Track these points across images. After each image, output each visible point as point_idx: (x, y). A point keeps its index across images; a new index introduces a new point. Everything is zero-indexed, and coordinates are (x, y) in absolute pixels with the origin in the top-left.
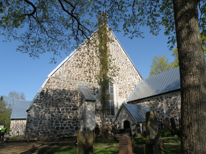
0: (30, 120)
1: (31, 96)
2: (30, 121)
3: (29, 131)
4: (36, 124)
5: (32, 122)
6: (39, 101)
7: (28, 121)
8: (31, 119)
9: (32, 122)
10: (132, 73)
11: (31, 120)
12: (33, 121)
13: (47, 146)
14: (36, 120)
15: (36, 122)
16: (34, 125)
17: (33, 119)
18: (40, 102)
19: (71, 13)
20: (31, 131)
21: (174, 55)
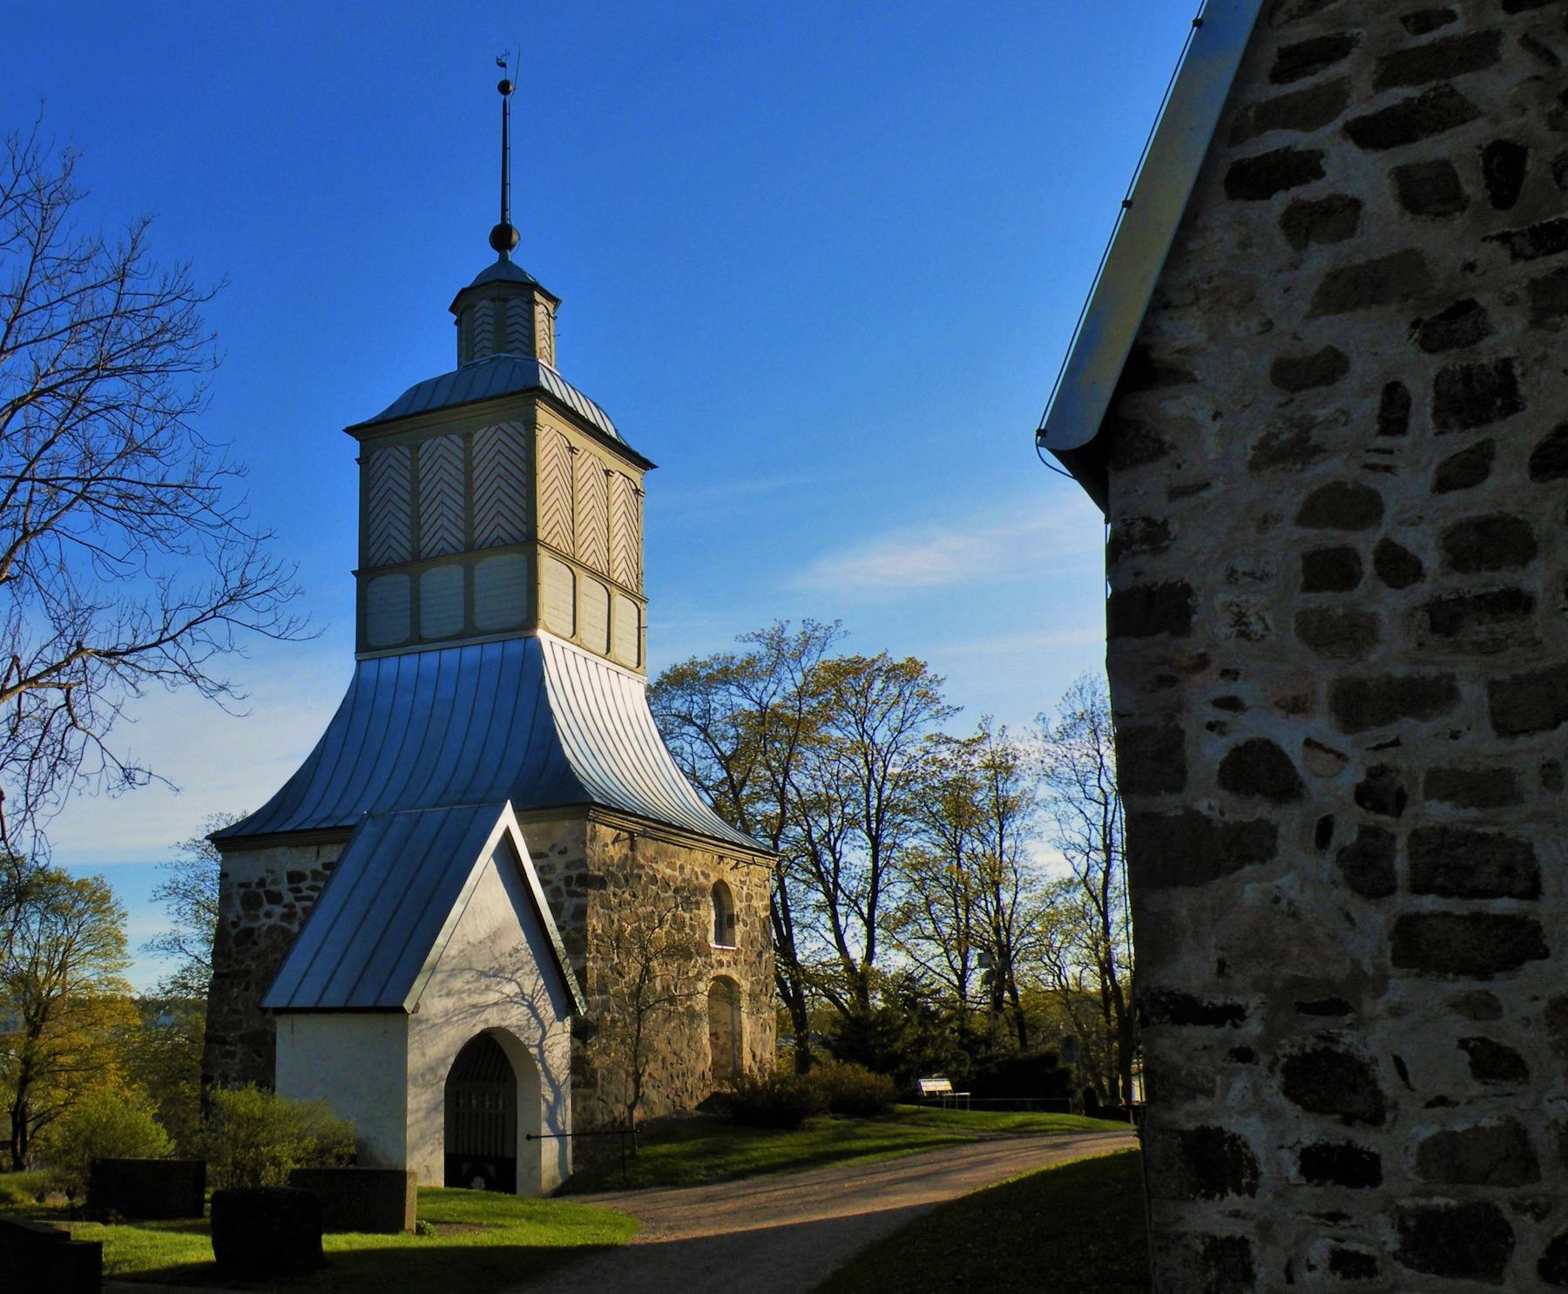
0: (1210, 753)
1: (1358, 809)
2: (1209, 801)
3: (1254, 1133)
4: (1445, 863)
5: (1290, 821)
6: (1359, 108)
7: (1168, 805)
8: (1246, 728)
9: (1290, 821)
10: (333, 1242)
11: (1259, 770)
12: (1333, 787)
13: (1408, 101)
14: (1422, 743)
15: (1439, 812)
16: (1377, 918)
17: (1321, 725)
18: (1444, 113)
19: (172, 605)
20: (1311, 1131)
21: (413, 1174)
